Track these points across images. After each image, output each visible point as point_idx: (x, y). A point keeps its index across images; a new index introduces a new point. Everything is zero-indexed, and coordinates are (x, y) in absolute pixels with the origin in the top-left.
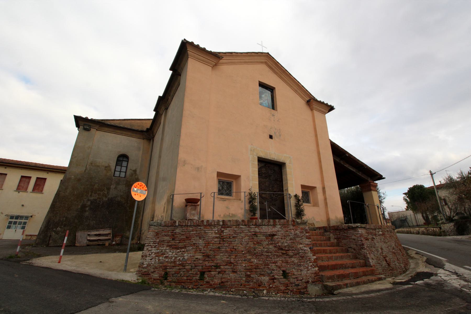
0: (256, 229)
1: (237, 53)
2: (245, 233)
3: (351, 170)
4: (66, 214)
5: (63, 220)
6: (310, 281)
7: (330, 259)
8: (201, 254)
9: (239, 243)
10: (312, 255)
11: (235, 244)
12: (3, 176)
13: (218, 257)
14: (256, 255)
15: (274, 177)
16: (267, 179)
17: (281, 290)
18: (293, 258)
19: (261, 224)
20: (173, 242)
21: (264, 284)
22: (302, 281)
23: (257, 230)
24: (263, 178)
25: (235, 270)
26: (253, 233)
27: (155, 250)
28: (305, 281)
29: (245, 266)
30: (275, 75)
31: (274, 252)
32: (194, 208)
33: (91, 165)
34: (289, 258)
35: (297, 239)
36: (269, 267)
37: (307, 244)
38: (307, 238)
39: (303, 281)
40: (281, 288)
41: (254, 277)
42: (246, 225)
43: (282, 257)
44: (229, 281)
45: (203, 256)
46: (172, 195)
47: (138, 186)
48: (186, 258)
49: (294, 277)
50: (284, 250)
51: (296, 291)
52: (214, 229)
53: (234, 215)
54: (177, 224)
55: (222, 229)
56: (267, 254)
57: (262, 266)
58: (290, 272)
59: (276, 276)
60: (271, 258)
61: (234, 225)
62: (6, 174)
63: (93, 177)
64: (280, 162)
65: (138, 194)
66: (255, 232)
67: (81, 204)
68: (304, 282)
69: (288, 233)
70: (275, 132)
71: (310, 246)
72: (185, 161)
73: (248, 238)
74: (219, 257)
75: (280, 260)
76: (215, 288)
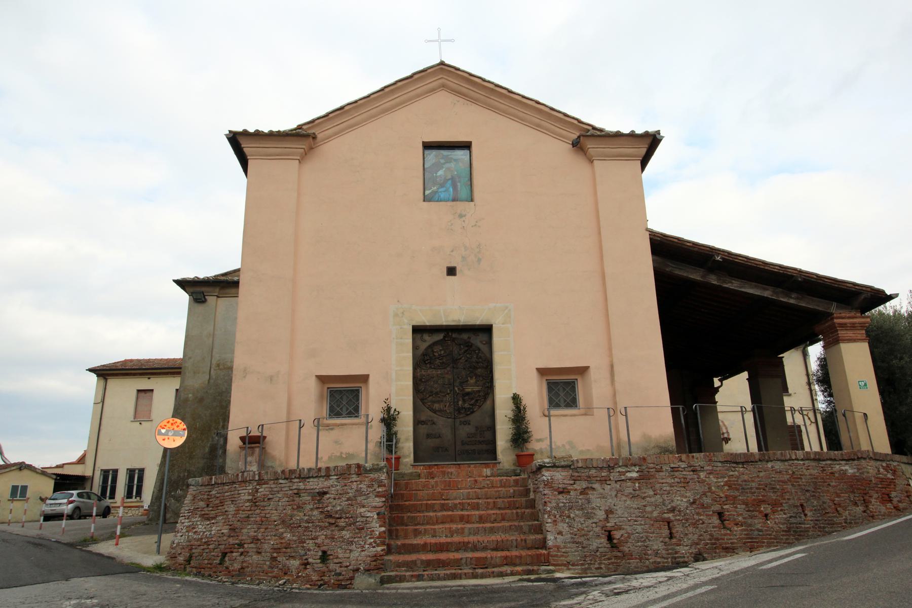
0: (301, 484)
1: (356, 102)
2: (284, 492)
3: (821, 283)
4: (187, 465)
5: (184, 476)
6: (362, 568)
7: (456, 532)
8: (227, 526)
9: (274, 509)
10: (378, 525)
11: (269, 511)
12: (148, 394)
13: (245, 531)
14: (291, 527)
15: (466, 361)
16: (448, 369)
17: (312, 581)
18: (345, 531)
19: (307, 476)
20: (206, 511)
21: (291, 571)
22: (349, 567)
23: (302, 486)
24: (435, 369)
25: (260, 551)
26: (296, 491)
27: (187, 522)
28: (353, 568)
29: (273, 545)
30: (474, 107)
31: (317, 521)
32: (251, 452)
33: (218, 368)
34: (339, 530)
35: (359, 499)
36: (305, 545)
37: (375, 507)
38: (376, 496)
39: (350, 567)
40: (313, 578)
41: (281, 560)
42: (287, 479)
43: (328, 529)
44: (250, 565)
45: (230, 529)
46: (261, 426)
47: (169, 425)
48: (213, 532)
49: (337, 562)
50: (334, 518)
51: (333, 583)
52: (248, 488)
53: (352, 455)
54: (213, 483)
55: (258, 487)
56: (307, 525)
57: (296, 544)
58: (333, 553)
59: (310, 560)
60: (311, 531)
61: (272, 480)
62: (152, 390)
63: (224, 390)
64: (475, 325)
65: (168, 439)
66: (299, 489)
67: (209, 445)
68: (351, 570)
69: (347, 489)
70: (463, 257)
71: (379, 509)
72: (245, 370)
73: (287, 499)
74: (246, 530)
75: (323, 535)
76: (233, 576)
